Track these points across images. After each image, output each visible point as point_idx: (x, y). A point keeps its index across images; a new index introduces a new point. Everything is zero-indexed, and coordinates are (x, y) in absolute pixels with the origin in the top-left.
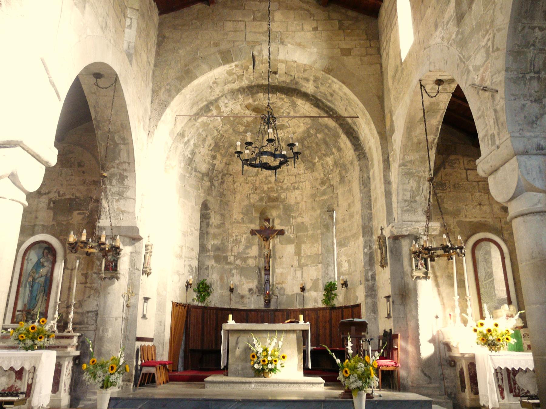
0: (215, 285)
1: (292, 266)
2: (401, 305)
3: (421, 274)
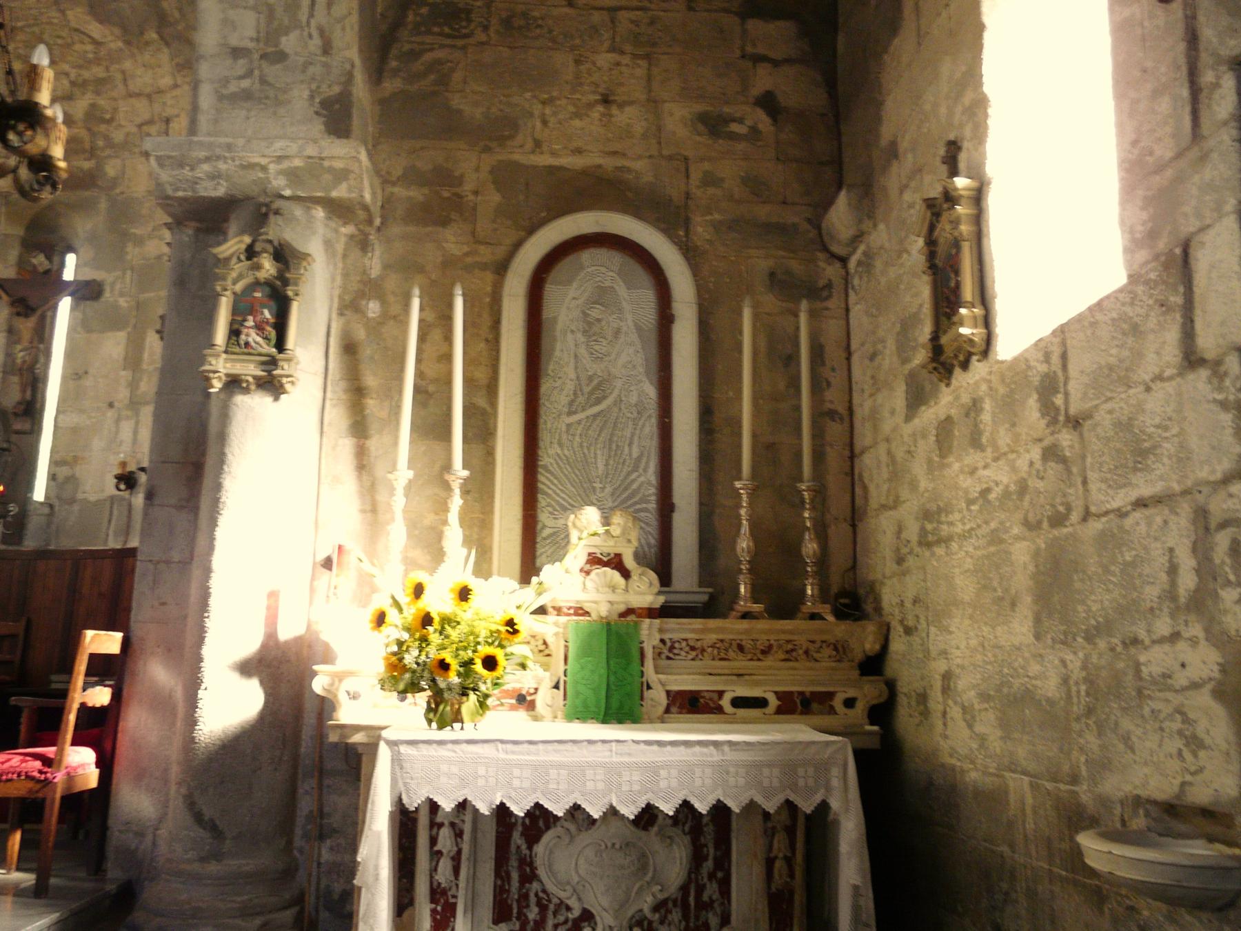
1: (111, 405)
2: (180, 508)
3: (249, 370)
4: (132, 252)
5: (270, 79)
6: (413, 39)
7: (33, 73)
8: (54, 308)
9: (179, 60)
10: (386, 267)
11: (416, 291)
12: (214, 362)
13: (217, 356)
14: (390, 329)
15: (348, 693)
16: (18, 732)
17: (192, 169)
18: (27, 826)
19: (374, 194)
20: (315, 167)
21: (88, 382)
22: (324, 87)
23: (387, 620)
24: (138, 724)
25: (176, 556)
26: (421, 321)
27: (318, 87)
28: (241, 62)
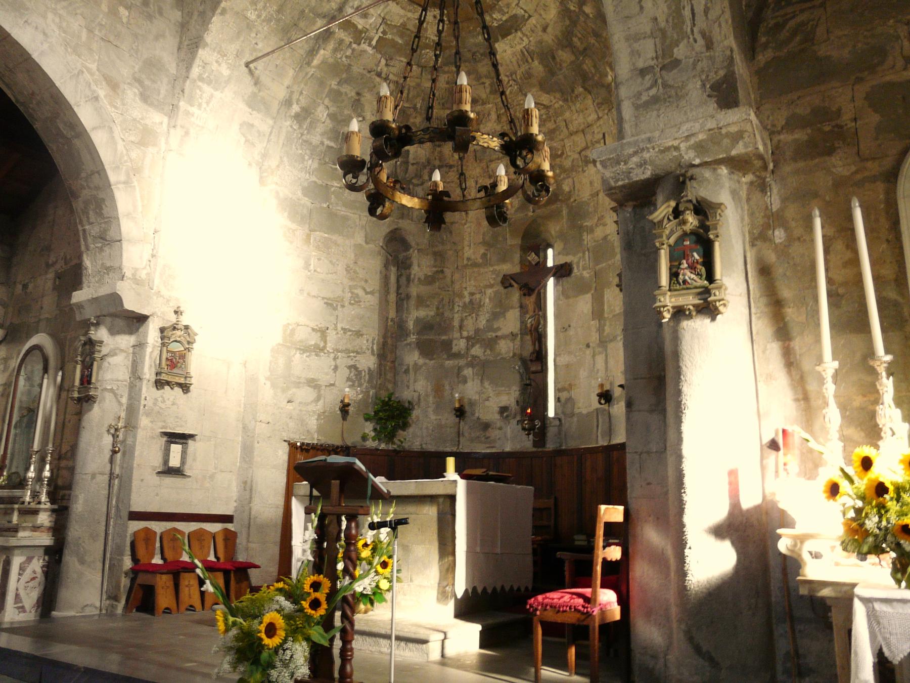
0: (423, 404)
1: (588, 346)
2: (651, 411)
3: (689, 300)
4: (587, 238)
5: (671, 82)
6: (777, 14)
7: (527, 113)
8: (545, 286)
9: (600, 100)
10: (784, 200)
11: (817, 212)
12: (662, 299)
13: (664, 294)
14: (796, 250)
15: (811, 553)
16: (564, 577)
17: (626, 163)
18: (580, 642)
19: (765, 145)
20: (716, 136)
21: (571, 332)
22: (712, 74)
23: (841, 490)
24: (642, 573)
25: (654, 447)
26: (823, 236)
27: (708, 76)
28: (647, 77)
